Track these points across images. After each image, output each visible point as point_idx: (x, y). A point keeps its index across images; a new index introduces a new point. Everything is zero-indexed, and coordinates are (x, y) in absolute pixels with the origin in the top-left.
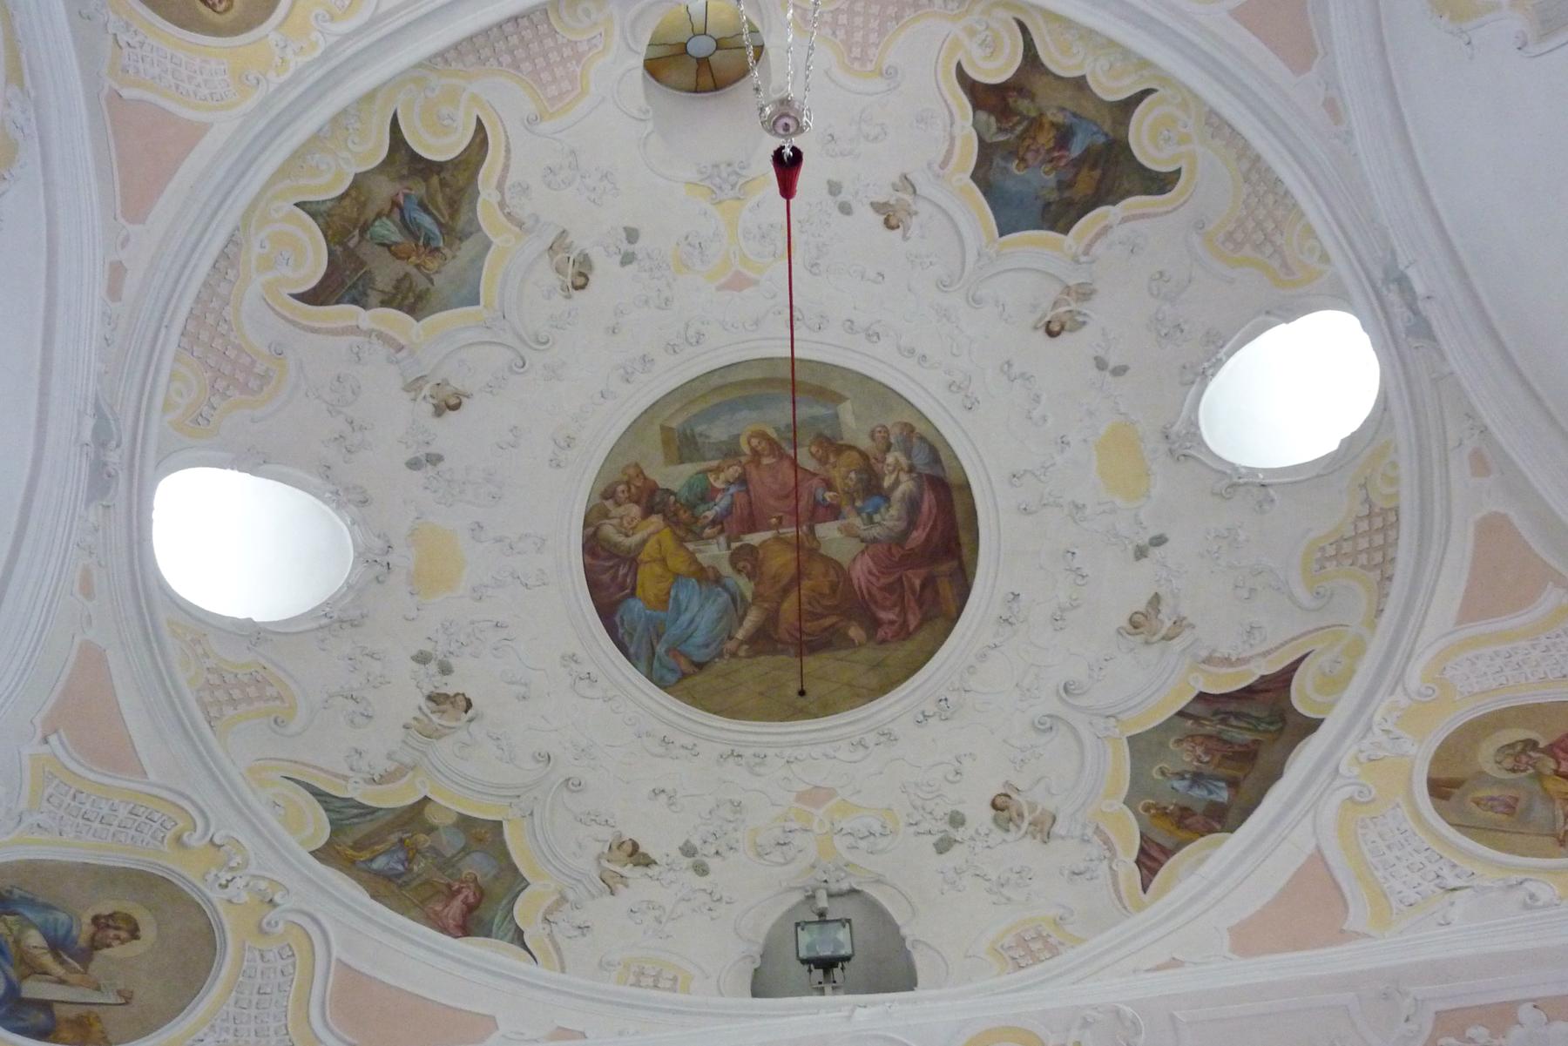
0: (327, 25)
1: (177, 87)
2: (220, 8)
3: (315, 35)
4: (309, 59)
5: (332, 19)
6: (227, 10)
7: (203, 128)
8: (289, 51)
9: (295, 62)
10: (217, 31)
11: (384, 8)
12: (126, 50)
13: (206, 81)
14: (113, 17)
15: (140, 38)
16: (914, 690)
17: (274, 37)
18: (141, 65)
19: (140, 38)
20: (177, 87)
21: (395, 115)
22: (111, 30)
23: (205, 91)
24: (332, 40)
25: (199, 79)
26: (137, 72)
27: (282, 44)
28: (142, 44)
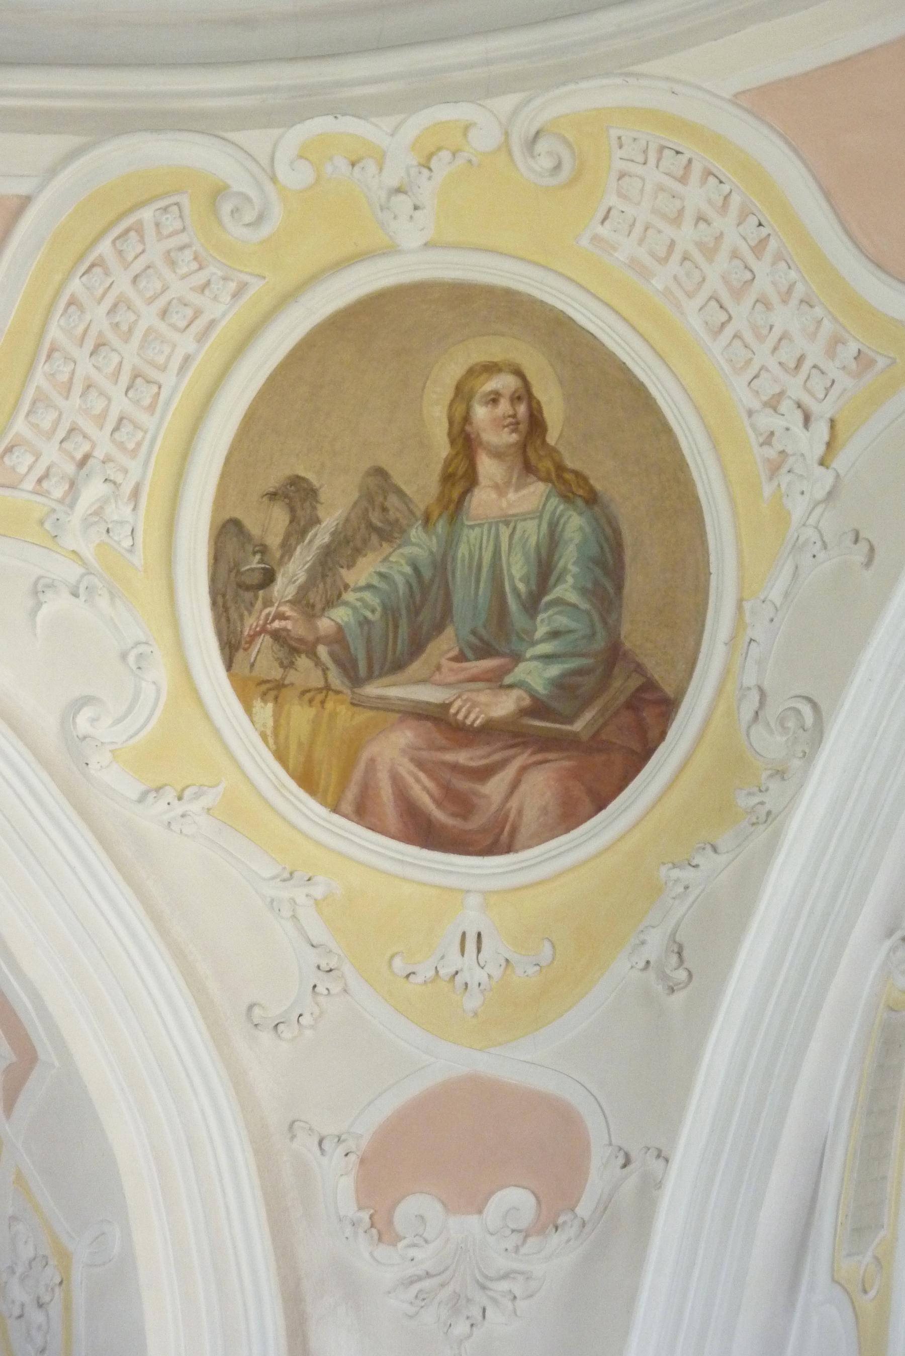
0: (240, 183)
1: (759, 248)
2: (505, 383)
3: (296, 176)
4: (350, 125)
5: (218, 193)
6: (491, 369)
7: (763, 101)
8: (392, 179)
9: (396, 137)
10: (556, 330)
11: (53, 145)
12: (823, 410)
13: (677, 220)
14: (798, 508)
15: (767, 421)
16: (18, 796)
17: (410, 233)
18: (815, 353)
19: (767, 421)
20: (759, 248)
21: (463, 954)
22: (826, 478)
23: (696, 195)
24: (256, 139)
25: (687, 235)
26: (836, 342)
27: (403, 203)
28: (773, 404)
